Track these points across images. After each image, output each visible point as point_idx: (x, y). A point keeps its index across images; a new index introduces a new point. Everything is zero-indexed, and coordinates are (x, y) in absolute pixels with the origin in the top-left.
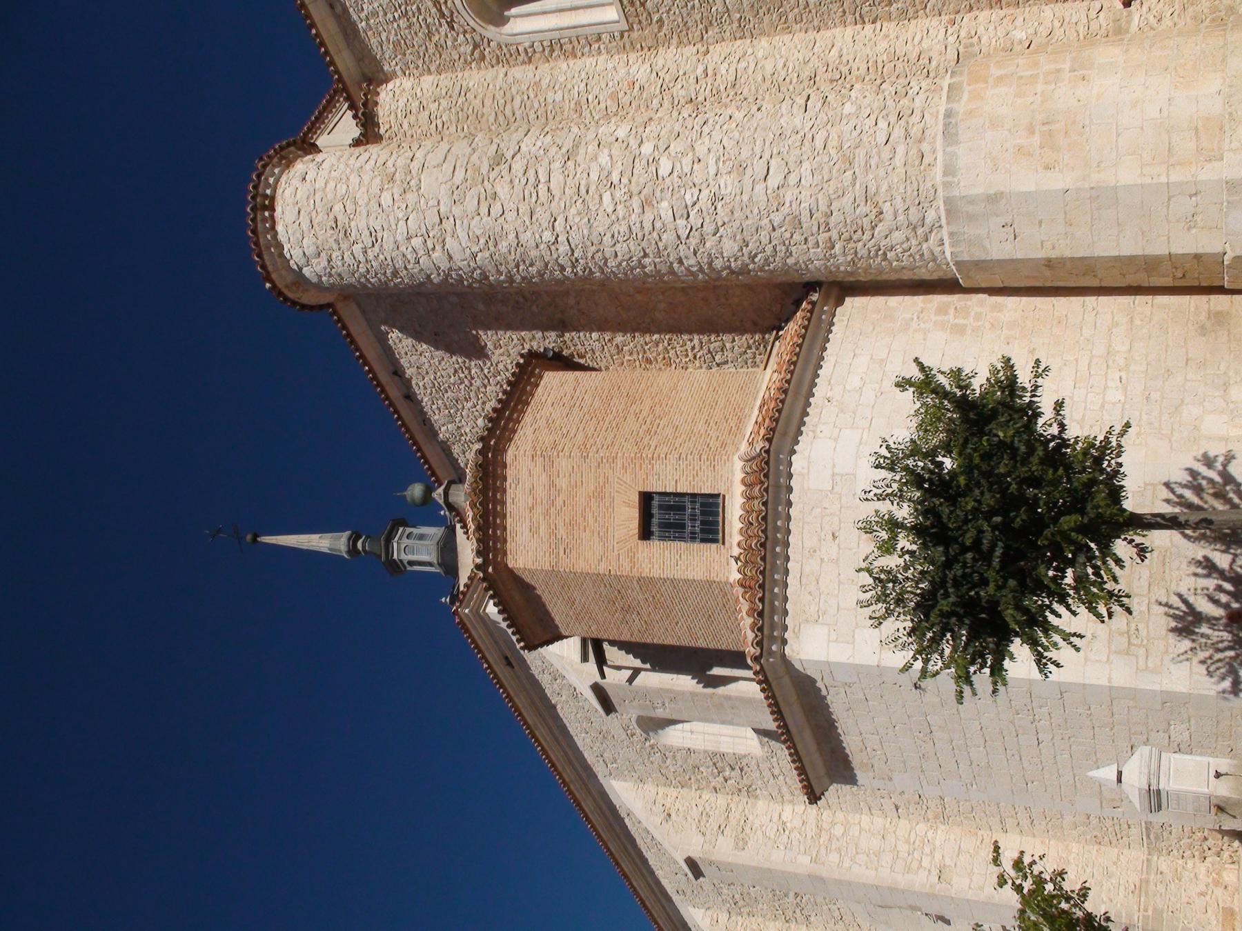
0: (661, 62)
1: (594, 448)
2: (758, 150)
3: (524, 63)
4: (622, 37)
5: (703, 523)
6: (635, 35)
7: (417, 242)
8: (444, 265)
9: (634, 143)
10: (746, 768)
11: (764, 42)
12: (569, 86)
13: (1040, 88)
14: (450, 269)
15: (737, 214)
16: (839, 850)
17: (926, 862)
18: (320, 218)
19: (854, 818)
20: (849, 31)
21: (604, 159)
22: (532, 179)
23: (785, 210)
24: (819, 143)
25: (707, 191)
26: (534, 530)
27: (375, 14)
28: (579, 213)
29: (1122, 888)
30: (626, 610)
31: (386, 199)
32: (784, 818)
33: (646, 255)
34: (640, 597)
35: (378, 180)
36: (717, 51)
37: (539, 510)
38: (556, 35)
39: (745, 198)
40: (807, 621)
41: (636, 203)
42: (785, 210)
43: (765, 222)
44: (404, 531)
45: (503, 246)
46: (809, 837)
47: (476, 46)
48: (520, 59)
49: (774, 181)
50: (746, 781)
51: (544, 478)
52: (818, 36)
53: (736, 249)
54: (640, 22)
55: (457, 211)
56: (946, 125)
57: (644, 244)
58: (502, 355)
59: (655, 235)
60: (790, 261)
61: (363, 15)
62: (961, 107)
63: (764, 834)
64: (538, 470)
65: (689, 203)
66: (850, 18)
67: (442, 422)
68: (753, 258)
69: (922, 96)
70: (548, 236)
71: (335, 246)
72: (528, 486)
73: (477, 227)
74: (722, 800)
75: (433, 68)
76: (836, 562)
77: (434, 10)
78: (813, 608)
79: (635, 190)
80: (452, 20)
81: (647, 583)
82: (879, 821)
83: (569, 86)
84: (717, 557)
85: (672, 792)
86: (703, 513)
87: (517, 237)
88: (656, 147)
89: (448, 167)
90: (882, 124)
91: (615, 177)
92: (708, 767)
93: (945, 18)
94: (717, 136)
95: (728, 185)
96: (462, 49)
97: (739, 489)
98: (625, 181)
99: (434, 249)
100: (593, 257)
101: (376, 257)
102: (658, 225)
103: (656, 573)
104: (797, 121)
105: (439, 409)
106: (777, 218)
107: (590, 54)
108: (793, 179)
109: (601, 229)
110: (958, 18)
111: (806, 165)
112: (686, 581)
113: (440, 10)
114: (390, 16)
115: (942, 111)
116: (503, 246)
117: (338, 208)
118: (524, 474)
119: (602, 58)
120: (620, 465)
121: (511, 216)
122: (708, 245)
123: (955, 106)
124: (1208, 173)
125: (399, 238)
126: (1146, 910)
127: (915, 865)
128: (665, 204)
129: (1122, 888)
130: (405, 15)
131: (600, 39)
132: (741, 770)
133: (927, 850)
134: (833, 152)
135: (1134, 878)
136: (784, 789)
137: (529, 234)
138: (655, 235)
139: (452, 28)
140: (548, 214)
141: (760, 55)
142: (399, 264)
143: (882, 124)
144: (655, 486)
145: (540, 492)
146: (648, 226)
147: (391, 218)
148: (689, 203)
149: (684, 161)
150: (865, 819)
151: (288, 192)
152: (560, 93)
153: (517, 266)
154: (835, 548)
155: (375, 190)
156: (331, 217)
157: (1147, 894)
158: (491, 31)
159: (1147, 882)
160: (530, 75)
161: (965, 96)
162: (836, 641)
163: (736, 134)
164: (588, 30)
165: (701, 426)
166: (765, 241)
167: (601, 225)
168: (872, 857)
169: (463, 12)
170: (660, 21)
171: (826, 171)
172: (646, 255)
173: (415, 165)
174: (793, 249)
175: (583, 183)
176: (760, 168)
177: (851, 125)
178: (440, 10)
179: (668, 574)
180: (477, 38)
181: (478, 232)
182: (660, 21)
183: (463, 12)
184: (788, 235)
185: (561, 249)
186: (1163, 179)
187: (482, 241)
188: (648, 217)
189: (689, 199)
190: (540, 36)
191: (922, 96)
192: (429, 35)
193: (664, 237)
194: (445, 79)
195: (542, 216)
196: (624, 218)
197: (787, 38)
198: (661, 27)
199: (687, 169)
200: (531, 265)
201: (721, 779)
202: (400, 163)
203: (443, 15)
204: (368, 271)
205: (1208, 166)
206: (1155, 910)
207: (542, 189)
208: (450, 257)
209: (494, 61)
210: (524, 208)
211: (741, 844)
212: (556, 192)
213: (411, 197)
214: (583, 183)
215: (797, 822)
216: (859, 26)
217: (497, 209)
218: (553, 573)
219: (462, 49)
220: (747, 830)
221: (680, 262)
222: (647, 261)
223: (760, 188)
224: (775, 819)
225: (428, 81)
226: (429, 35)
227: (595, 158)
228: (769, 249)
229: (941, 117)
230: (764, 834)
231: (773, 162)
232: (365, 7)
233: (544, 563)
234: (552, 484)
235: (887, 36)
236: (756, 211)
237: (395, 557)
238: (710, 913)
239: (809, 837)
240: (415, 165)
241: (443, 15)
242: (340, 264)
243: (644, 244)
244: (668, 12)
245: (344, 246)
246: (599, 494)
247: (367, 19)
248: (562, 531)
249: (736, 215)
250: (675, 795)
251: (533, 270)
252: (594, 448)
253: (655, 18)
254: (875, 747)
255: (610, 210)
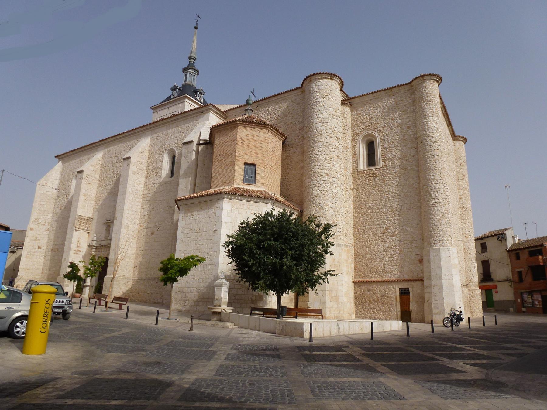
0: (350, 178)
1: (267, 153)
2: (337, 202)
3: (352, 145)
4: (356, 169)
5: (248, 179)
6: (356, 172)
7: (321, 116)
8: (314, 121)
9: (340, 173)
10: (156, 176)
11: (352, 203)
12: (347, 155)
13: (346, 264)
14: (313, 123)
15: (324, 196)
16: (132, 199)
17: (129, 223)
18: (328, 91)
19: (140, 204)
20: (353, 222)
21: (337, 165)
22: (334, 147)
23: (324, 207)
24: (338, 216)
25: (329, 189)
26: (247, 135)
27: (368, 110)
28: (326, 158)
29: (124, 272)
30: (224, 156)
31: (331, 109)
32: (140, 185)
33: (314, 172)
34: (228, 161)
35: (336, 108)
36: (351, 191)
37: (252, 137)
38: (358, 154)
39: (327, 198)
40: (232, 205)
41: (328, 172)
42: (324, 207)
43: (321, 202)
44: (196, 74)
45: (318, 138)
46: (136, 192)
47: (357, 134)
48: (353, 144)
49: (330, 205)
50: (151, 176)
51: (260, 139)
52: (352, 215)
53: (315, 194)
54: (359, 174)
55: (328, 127)
56: (340, 244)
57: (317, 173)
58: (284, 129)
59: (320, 176)
60: (311, 207)
61: (368, 107)
62: (343, 247)
63: (137, 179)
64: (262, 138)
65: (327, 185)
66: (355, 222)
67: (264, 109)
68: (312, 198)
69: (345, 239)
70: (321, 149)
71: (321, 94)
72: (258, 135)
73: (324, 132)
74: (145, 168)
75: (353, 122)
76: (246, 213)
77: (367, 125)
78: (235, 207)
79: (330, 172)
80: (364, 129)
81: (233, 164)
82: (139, 211)
83: (347, 155)
84: (240, 182)
85: (147, 154)
86: (250, 179)
87: (321, 141)
88: (339, 178)
89: (337, 126)
90: (341, 230)
91: (333, 167)
92: (156, 166)
93: (353, 243)
94: (340, 192)
95: (330, 194)
96: (357, 130)
97: (257, 189)
98: (333, 170)
99: (319, 120)
100: (314, 159)
101: (317, 104)
102: (322, 177)
103: (236, 166)
104: (342, 211)
105: (268, 109)
106: (322, 205)
107: (353, 161)
108: (330, 209)
109: (321, 162)
110: (353, 246)
111: (333, 212)
112: (234, 173)
113: (367, 127)
114: (367, 114)
115: (343, 243)
116: (318, 138)
117: (330, 97)
118: (261, 134)
119: (352, 164)
120: (263, 160)
121: (326, 141)
122: (316, 188)
123: (344, 246)
124: (328, 298)
125: (322, 111)
126: (119, 278)
127: (129, 220)
128: (327, 179)
129: (124, 272)
130: (367, 118)
131: (356, 164)
132: (156, 175)
133: (132, 223)
134: (336, 219)
135: (126, 276)
136: (149, 186)
137: (321, 144)
138: (320, 176)
139: (362, 129)
140: (326, 150)
141: (350, 202)
142: (315, 110)
143: (341, 230)
144: (258, 168)
145: (257, 138)
146: (322, 174)
147: (327, 110)
148: (327, 185)
149: (336, 184)
150: (140, 207)
151: (334, 84)
152: (345, 153)
153: (313, 140)
154: (249, 213)
155: (334, 107)
156: (328, 94)
157: (123, 278)
158: (361, 138)
159: (126, 279)
160: (350, 146)
161: (345, 249)
162: (228, 212)
163: (341, 197)
164: (358, 162)
165: (270, 181)
166: (317, 201)
167: (323, 163)
168: (131, 208)
169: (366, 132)
170: (359, 179)
171: (332, 217)
172: (314, 172)
173: (338, 118)
174: (314, 208)
175: (333, 160)
176: (333, 202)
177: (341, 223)
178: (367, 127)
179: (236, 169)
180: (359, 134)
181: (322, 132)
182: (359, 179)
183: (366, 132)
184: (318, 207)
185: (317, 152)
186: (327, 289)
187: (320, 132)
188: (324, 175)
189: (327, 185)
190: (358, 150)
191: (345, 239)
192: (361, 123)
193: (319, 178)
194: (350, 124)
195: (326, 148)
196: (324, 169)
197: (352, 208)
198: (357, 179)
199: (334, 185)
200: (313, 144)
201: (152, 169)
202: (339, 114)
203: (366, 127)
204: (313, 101)
205: (329, 298)
206: (119, 280)
207: (332, 150)
208: (316, 123)
209: (353, 137)
210: (328, 144)
211: (134, 173)
212: (331, 153)
213: (331, 116)
214: (333, 160)
215: (139, 189)
216: (353, 224)
217: (328, 137)
218: (236, 139)
219: (357, 130)
220: (138, 175)
221: (312, 180)
222: (313, 173)
223: (329, 202)
224: (140, 183)
225: (350, 120)
226: (361, 123)
227: (338, 163)
228: (314, 202)
229: (342, 243)
230: (137, 179)
231: (334, 205)
232: (370, 108)
233: (239, 137)
234: (259, 142)
235: (351, 230)
236: (324, 200)
237: (189, 71)
238: (102, 159)
239: (136, 192)
240: (338, 118)
241: (366, 127)
242: (316, 94)
243: (317, 173)
244: (361, 181)
245: (321, 96)
246: (256, 153)
247: (367, 108)
248: (247, 142)
249: (323, 195)
250: (146, 155)
251: (312, 144)
252: (267, 153)
253: (360, 178)
254: (194, 218)
255: (326, 165)
